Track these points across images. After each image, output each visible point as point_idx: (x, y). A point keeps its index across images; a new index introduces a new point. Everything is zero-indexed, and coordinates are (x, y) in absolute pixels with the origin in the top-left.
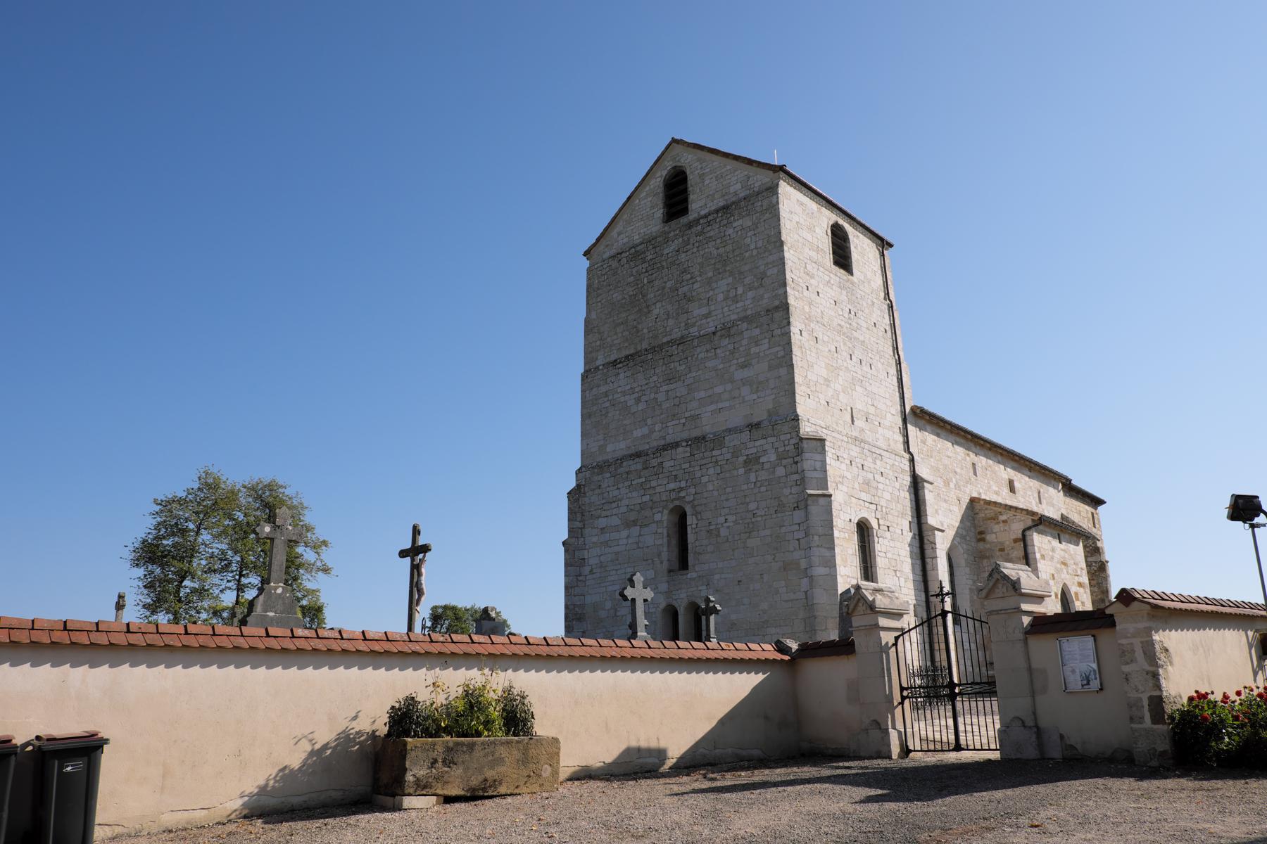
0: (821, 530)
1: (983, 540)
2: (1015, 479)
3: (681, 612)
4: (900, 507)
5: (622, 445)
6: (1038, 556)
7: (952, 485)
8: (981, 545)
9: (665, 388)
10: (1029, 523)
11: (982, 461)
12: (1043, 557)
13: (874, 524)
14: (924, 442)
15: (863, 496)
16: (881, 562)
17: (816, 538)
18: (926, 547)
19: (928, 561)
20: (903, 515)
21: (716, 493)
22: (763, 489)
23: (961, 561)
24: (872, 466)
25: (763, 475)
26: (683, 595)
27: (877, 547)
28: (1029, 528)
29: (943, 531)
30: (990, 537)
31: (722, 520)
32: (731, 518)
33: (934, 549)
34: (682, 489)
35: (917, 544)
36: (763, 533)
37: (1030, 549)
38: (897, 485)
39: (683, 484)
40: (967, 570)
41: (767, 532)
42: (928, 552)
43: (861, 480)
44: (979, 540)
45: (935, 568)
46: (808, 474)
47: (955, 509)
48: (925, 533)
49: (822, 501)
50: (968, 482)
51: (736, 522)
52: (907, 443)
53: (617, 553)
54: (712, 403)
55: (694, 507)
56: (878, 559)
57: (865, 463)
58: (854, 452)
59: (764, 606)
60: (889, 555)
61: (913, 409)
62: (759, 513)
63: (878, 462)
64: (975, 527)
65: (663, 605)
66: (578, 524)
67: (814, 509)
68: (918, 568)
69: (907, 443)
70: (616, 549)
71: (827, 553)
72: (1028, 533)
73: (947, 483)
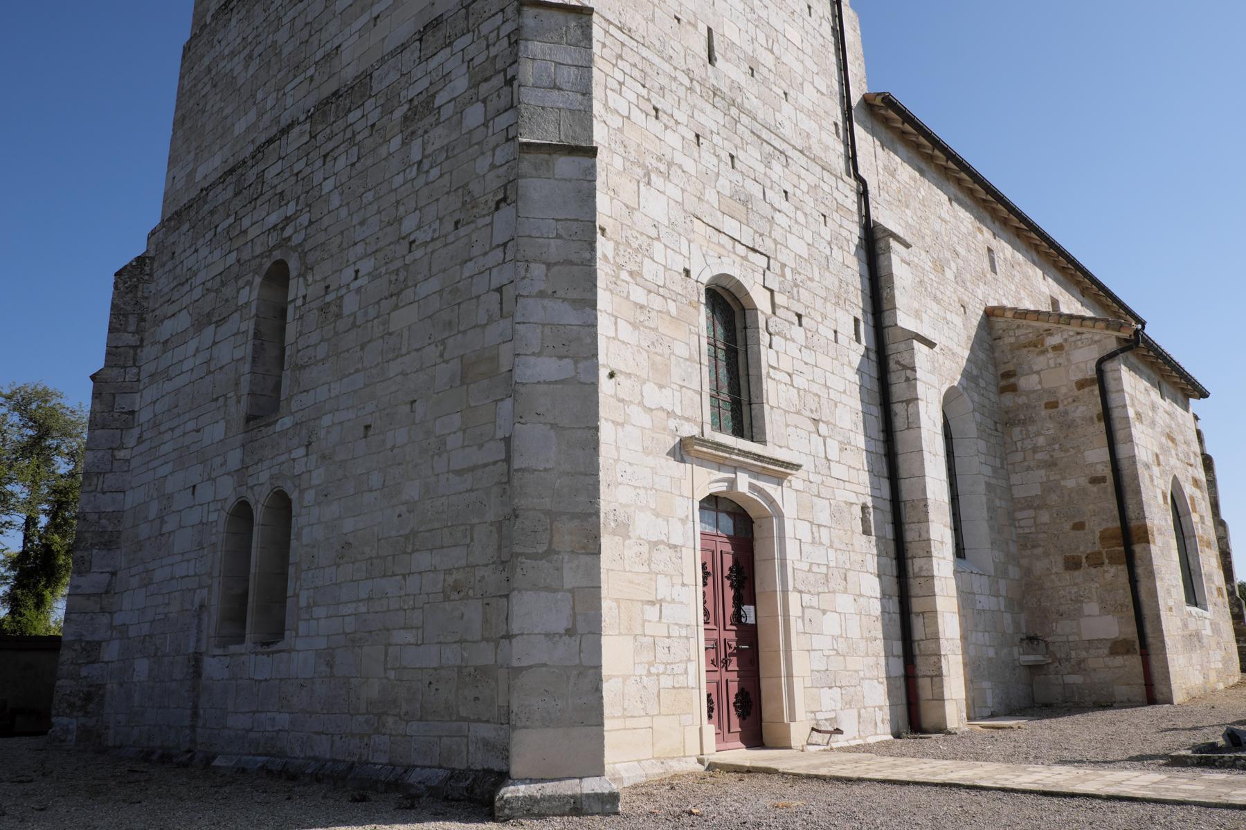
0: (554, 249)
1: (1013, 388)
2: (1060, 299)
3: (259, 514)
4: (831, 281)
5: (217, 161)
6: (1131, 413)
7: (949, 274)
8: (1008, 400)
9: (291, 14)
10: (1112, 345)
11: (1006, 251)
12: (1139, 415)
13: (761, 300)
14: (893, 174)
15: (731, 226)
16: (776, 394)
17: (538, 270)
18: (893, 378)
19: (898, 408)
20: (840, 300)
21: (344, 212)
22: (435, 172)
23: (968, 427)
24: (760, 168)
25: (439, 138)
26: (264, 477)
27: (767, 357)
28: (1112, 356)
29: (931, 345)
30: (1027, 382)
31: (349, 273)
32: (366, 266)
33: (911, 381)
34: (288, 220)
35: (873, 370)
36: (426, 288)
37: (1114, 399)
38: (826, 233)
39: (291, 209)
40: (982, 445)
41: (433, 285)
42: (898, 390)
43: (724, 185)
44: (1003, 390)
45: (913, 424)
46: (529, 97)
47: (958, 320)
48: (892, 348)
49: (565, 165)
50: (981, 277)
51: (374, 276)
52: (852, 158)
53: (178, 391)
54: (363, 10)
55: (303, 256)
56: (769, 387)
57: (741, 155)
58: (710, 118)
59: (412, 491)
60: (799, 381)
61: (867, 102)
62: (421, 236)
63: (777, 167)
64: (996, 365)
65: (232, 502)
66: (132, 339)
67: (539, 190)
68: (876, 425)
69: (852, 158)
70: (178, 382)
71: (570, 317)
72: (1109, 366)
73: (940, 266)
